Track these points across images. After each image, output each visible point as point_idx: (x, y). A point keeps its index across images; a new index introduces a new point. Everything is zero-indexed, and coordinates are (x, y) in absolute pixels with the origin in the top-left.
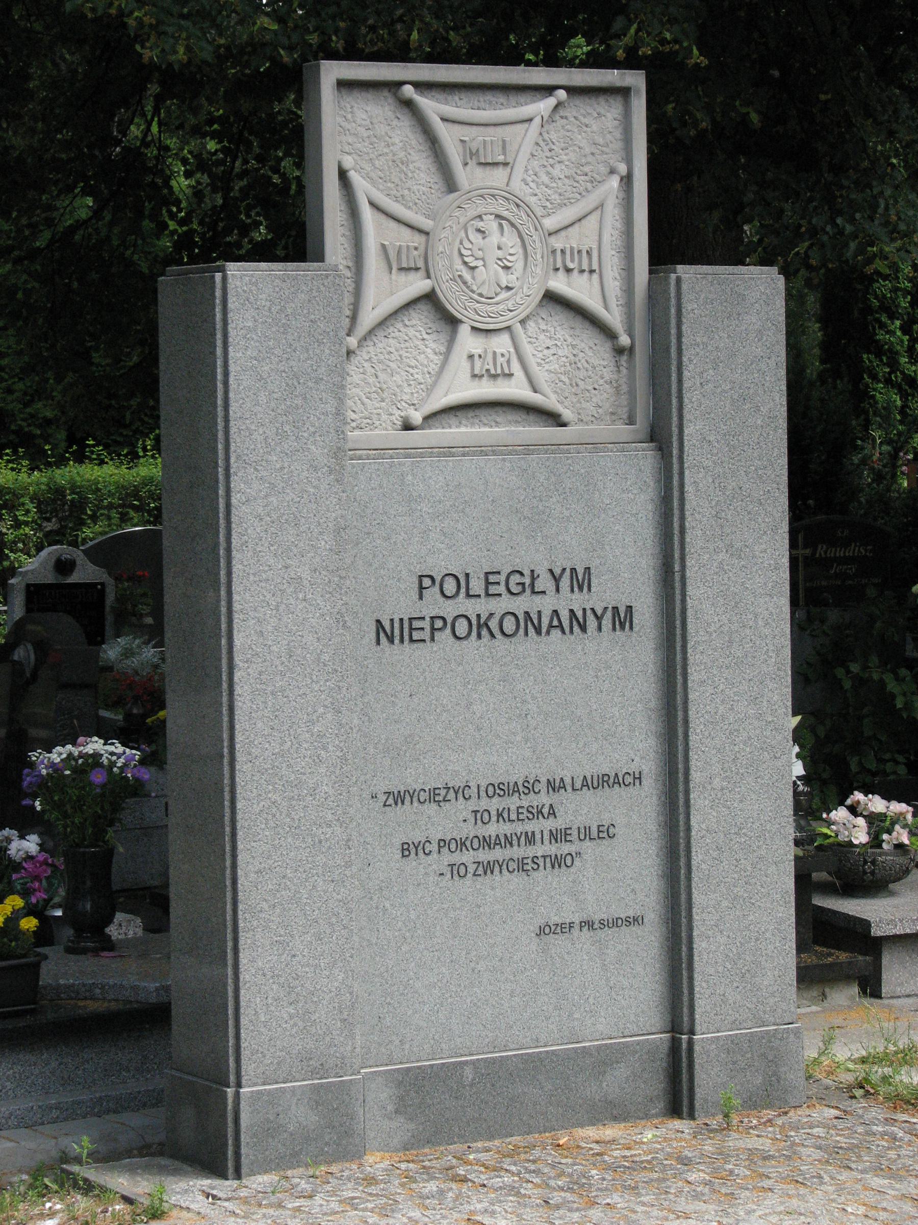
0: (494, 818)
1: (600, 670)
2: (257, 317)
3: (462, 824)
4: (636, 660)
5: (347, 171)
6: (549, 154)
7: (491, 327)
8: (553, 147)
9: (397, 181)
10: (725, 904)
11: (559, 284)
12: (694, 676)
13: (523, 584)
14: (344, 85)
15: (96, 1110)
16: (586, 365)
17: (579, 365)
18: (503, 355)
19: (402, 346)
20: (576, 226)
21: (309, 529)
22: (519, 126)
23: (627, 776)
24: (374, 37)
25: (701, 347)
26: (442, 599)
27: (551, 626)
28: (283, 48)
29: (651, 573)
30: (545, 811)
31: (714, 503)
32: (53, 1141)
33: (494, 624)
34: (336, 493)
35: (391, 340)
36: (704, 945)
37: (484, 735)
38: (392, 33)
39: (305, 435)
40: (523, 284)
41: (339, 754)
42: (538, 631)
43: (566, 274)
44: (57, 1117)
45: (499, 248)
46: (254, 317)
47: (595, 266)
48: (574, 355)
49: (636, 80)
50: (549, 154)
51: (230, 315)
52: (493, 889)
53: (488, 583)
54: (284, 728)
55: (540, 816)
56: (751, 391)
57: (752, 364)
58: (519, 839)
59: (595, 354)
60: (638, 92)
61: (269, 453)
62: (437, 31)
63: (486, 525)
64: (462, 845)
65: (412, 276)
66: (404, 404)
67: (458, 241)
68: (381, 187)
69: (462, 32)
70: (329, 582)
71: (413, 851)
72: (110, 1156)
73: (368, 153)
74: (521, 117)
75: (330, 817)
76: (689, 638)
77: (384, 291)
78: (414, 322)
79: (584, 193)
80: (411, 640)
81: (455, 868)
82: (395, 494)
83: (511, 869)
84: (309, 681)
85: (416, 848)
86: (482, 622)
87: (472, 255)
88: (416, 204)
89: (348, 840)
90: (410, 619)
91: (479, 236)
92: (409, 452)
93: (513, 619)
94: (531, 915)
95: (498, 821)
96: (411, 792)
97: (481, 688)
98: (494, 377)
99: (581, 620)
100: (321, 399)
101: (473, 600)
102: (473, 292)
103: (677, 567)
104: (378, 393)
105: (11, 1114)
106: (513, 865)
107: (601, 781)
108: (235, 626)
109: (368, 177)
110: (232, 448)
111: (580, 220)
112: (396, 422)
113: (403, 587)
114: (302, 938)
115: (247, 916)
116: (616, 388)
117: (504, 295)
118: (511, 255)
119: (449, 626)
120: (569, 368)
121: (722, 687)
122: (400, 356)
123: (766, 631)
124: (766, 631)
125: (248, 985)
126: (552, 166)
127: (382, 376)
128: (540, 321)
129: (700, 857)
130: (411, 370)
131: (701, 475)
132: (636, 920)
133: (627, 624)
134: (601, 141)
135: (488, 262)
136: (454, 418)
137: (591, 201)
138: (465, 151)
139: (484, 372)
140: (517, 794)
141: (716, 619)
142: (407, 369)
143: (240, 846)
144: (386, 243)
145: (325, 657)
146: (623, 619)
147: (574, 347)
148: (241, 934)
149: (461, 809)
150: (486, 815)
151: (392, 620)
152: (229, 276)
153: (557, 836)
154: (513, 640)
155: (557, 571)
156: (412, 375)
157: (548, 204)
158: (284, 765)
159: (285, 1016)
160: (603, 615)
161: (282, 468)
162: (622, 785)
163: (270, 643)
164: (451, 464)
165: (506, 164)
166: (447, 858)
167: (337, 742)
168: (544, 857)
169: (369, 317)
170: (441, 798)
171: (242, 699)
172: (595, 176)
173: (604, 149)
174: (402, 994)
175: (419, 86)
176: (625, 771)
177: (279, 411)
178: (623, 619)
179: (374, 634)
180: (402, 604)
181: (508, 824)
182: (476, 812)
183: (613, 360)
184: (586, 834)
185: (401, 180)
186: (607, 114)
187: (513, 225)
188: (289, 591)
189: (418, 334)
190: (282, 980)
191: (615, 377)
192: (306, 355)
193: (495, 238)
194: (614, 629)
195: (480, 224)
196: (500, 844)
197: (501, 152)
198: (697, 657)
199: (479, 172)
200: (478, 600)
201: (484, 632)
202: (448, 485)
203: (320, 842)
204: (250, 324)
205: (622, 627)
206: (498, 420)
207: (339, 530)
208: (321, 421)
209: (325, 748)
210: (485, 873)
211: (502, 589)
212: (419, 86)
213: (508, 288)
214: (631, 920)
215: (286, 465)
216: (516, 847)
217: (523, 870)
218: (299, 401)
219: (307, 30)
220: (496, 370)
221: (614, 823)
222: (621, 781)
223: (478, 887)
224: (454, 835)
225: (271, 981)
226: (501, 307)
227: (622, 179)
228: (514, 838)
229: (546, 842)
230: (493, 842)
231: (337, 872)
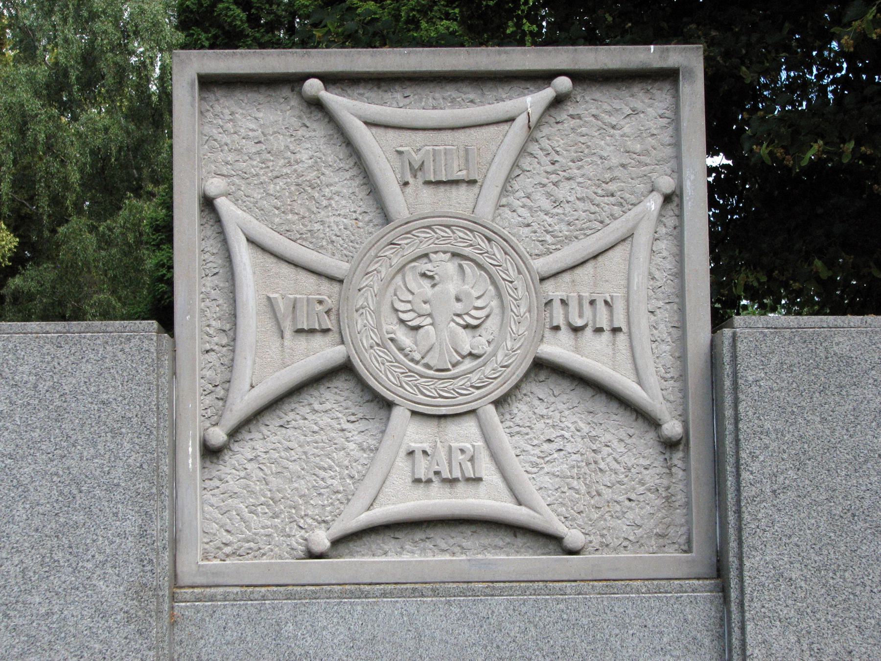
2: (14, 398)
5: (214, 199)
6: (550, 168)
7: (443, 411)
8: (557, 158)
11: (559, 349)
14: (208, 83)
16: (615, 465)
17: (602, 465)
18: (462, 451)
19: (308, 439)
20: (590, 266)
22: (492, 129)
34: (138, 651)
35: (290, 432)
39: (89, 565)
43: (572, 335)
45: (458, 300)
46: (9, 397)
47: (620, 321)
49: (689, 59)
50: (550, 168)
56: (866, 503)
57: (866, 461)
59: (626, 450)
65: (318, 340)
66: (310, 521)
73: (257, 175)
78: (328, 406)
79: (607, 221)
82: (265, 651)
88: (333, 242)
91: (426, 283)
92: (317, 590)
98: (452, 482)
100: (116, 514)
102: (417, 363)
104: (268, 506)
111: (595, 257)
112: (295, 545)
117: (468, 364)
120: (585, 469)
126: (555, 184)
127: (274, 481)
128: (537, 402)
130: (322, 473)
131: (775, 631)
134: (638, 147)
135: (438, 319)
136: (393, 541)
137: (615, 230)
138: (403, 166)
139: (431, 475)
142: (317, 471)
144: (271, 296)
147: (594, 439)
156: (323, 479)
157: (548, 238)
164: (359, 608)
165: (473, 182)
172: (627, 196)
175: (330, 80)
177: (47, 531)
183: (661, 458)
185: (309, 210)
186: (648, 108)
189: (334, 423)
191: (665, 482)
192: (92, 451)
193: (452, 287)
197: (462, 167)
199: (427, 193)
202: (353, 640)
206: (465, 544)
208: (114, 546)
212: (330, 80)
213: (473, 356)
215: (56, 609)
218: (80, 517)
227: (668, 199)
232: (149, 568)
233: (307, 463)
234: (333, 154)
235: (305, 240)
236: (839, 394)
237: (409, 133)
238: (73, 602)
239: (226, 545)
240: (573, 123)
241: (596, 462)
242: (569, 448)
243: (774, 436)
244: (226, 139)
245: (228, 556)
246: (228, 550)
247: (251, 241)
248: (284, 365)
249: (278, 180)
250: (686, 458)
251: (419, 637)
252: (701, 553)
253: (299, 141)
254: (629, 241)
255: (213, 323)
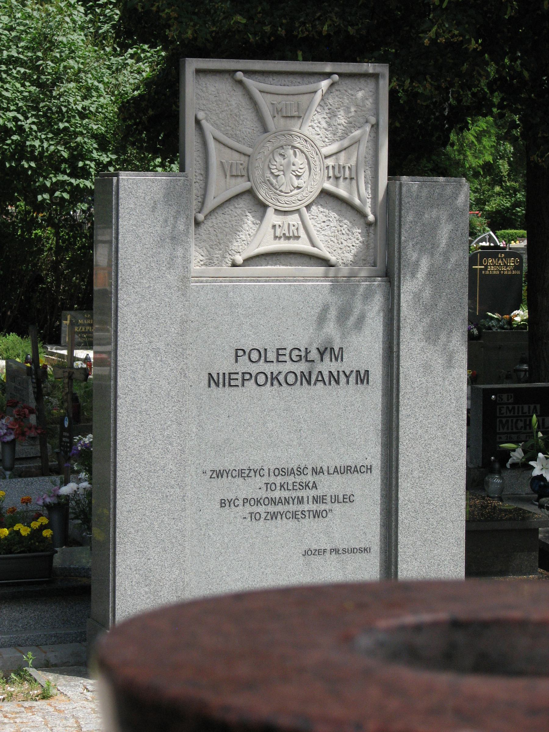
0: (278, 488)
1: (347, 406)
3: (258, 490)
4: (370, 401)
9: (232, 126)
10: (419, 543)
12: (403, 412)
13: (300, 356)
14: (199, 72)
15: (78, 639)
16: (348, 232)
17: (344, 232)
18: (294, 226)
21: (165, 321)
23: (362, 467)
24: (304, 28)
25: (413, 223)
26: (250, 363)
27: (317, 380)
28: (251, 34)
29: (381, 351)
30: (311, 485)
31: (419, 313)
32: (44, 655)
33: (281, 378)
34: (182, 302)
36: (404, 566)
37: (274, 440)
38: (314, 26)
39: (164, 268)
40: (308, 185)
41: (179, 448)
42: (309, 383)
44: (55, 641)
47: (353, 175)
48: (341, 226)
49: (383, 69)
51: (120, 201)
52: (276, 527)
53: (278, 355)
54: (147, 432)
55: (307, 488)
58: (293, 500)
60: (383, 76)
61: (142, 278)
62: (339, 25)
63: (278, 322)
64: (258, 502)
65: (239, 180)
66: (233, 252)
67: (268, 160)
68: (223, 129)
69: (356, 27)
70: (177, 351)
71: (227, 504)
72: (46, 666)
73: (215, 110)
74: (309, 91)
75: (173, 482)
76: (401, 390)
77: (220, 188)
78: (241, 206)
80: (230, 385)
81: (253, 515)
83: (288, 517)
84: (162, 406)
85: (230, 502)
86: (274, 377)
87: (276, 169)
88: (244, 139)
89: (184, 496)
90: (229, 373)
93: (293, 375)
94: (300, 544)
95: (281, 490)
96: (227, 471)
97: (273, 413)
98: (289, 238)
99: (336, 377)
101: (269, 364)
102: (277, 189)
103: (395, 350)
105: (28, 638)
106: (289, 515)
107: (346, 470)
108: (118, 374)
109: (214, 124)
110: (120, 275)
112: (228, 262)
113: (225, 355)
114: (154, 550)
115: (121, 535)
116: (367, 245)
117: (296, 191)
118: (300, 168)
119: (253, 378)
120: (337, 233)
121: (421, 419)
122: (232, 225)
123: (451, 388)
124: (451, 388)
125: (121, 574)
129: (404, 516)
132: (366, 550)
133: (365, 381)
138: (274, 110)
139: (282, 235)
140: (293, 475)
141: (418, 380)
143: (118, 497)
144: (223, 161)
145: (173, 393)
146: (363, 378)
148: (117, 545)
149: (259, 481)
150: (273, 486)
151: (218, 374)
152: (120, 179)
153: (316, 500)
154: (293, 387)
155: (322, 349)
157: (326, 140)
158: (146, 453)
159: (142, 592)
160: (350, 375)
161: (149, 287)
162: (359, 473)
163: (139, 384)
166: (248, 509)
167: (179, 441)
168: (309, 511)
169: (211, 203)
170: (246, 475)
171: (121, 415)
173: (363, 108)
174: (218, 584)
175: (246, 72)
176: (361, 464)
178: (363, 378)
179: (207, 382)
180: (224, 365)
181: (287, 491)
182: (267, 484)
184: (335, 499)
185: (235, 126)
187: (302, 152)
188: (152, 355)
190: (141, 572)
194: (357, 383)
195: (282, 151)
196: (282, 502)
198: (405, 401)
199: (282, 121)
200: (272, 364)
201: (275, 382)
203: (167, 496)
204: (132, 206)
205: (362, 382)
207: (183, 322)
209: (171, 444)
210: (272, 519)
211: (287, 358)
212: (246, 72)
213: (299, 188)
214: (363, 550)
216: (291, 505)
217: (296, 518)
219: (264, 24)
220: (289, 233)
221: (353, 494)
222: (359, 470)
223: (267, 526)
224: (253, 496)
225: (135, 572)
226: (293, 198)
227: (372, 126)
228: (291, 499)
229: (310, 503)
230: (277, 501)
231: (177, 514)
232: (186, 270)
233: (232, 228)
234: (244, 102)
235: (234, 138)
236: (437, 208)
237: (276, 96)
238: (158, 282)
239: (201, 261)
240: (338, 93)
241: (341, 231)
242: (332, 225)
243: (413, 223)
244: (203, 95)
245: (202, 265)
246: (202, 263)
247: (215, 138)
248: (227, 190)
249: (223, 113)
250: (375, 230)
251: (279, 298)
252: (380, 265)
253: (231, 96)
254: (358, 143)
255: (197, 171)
